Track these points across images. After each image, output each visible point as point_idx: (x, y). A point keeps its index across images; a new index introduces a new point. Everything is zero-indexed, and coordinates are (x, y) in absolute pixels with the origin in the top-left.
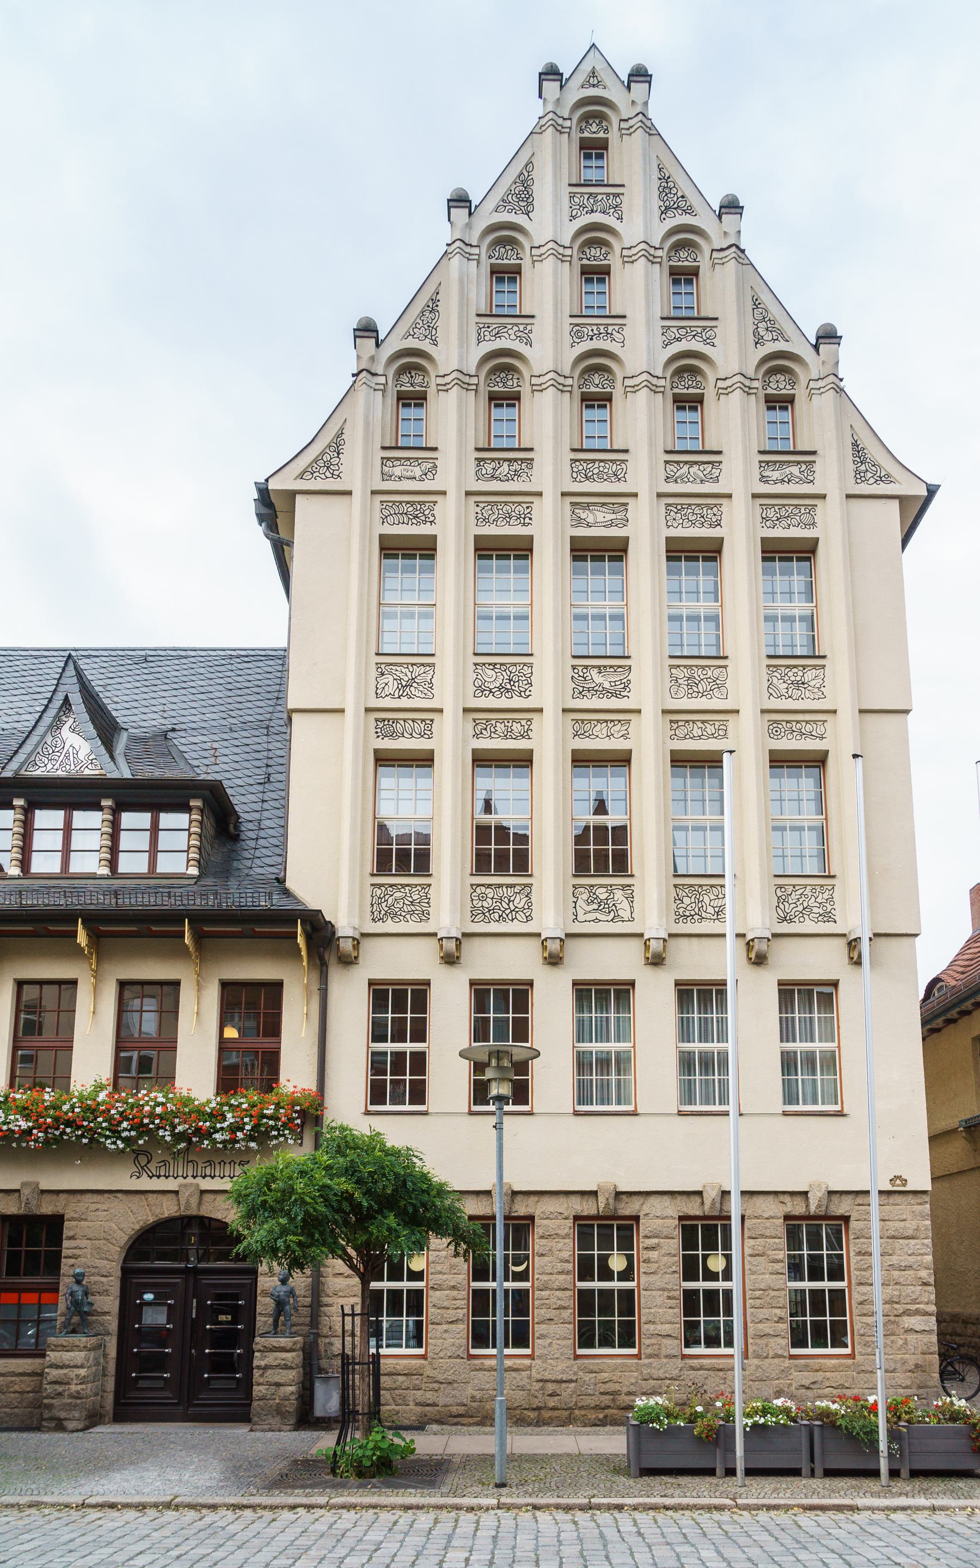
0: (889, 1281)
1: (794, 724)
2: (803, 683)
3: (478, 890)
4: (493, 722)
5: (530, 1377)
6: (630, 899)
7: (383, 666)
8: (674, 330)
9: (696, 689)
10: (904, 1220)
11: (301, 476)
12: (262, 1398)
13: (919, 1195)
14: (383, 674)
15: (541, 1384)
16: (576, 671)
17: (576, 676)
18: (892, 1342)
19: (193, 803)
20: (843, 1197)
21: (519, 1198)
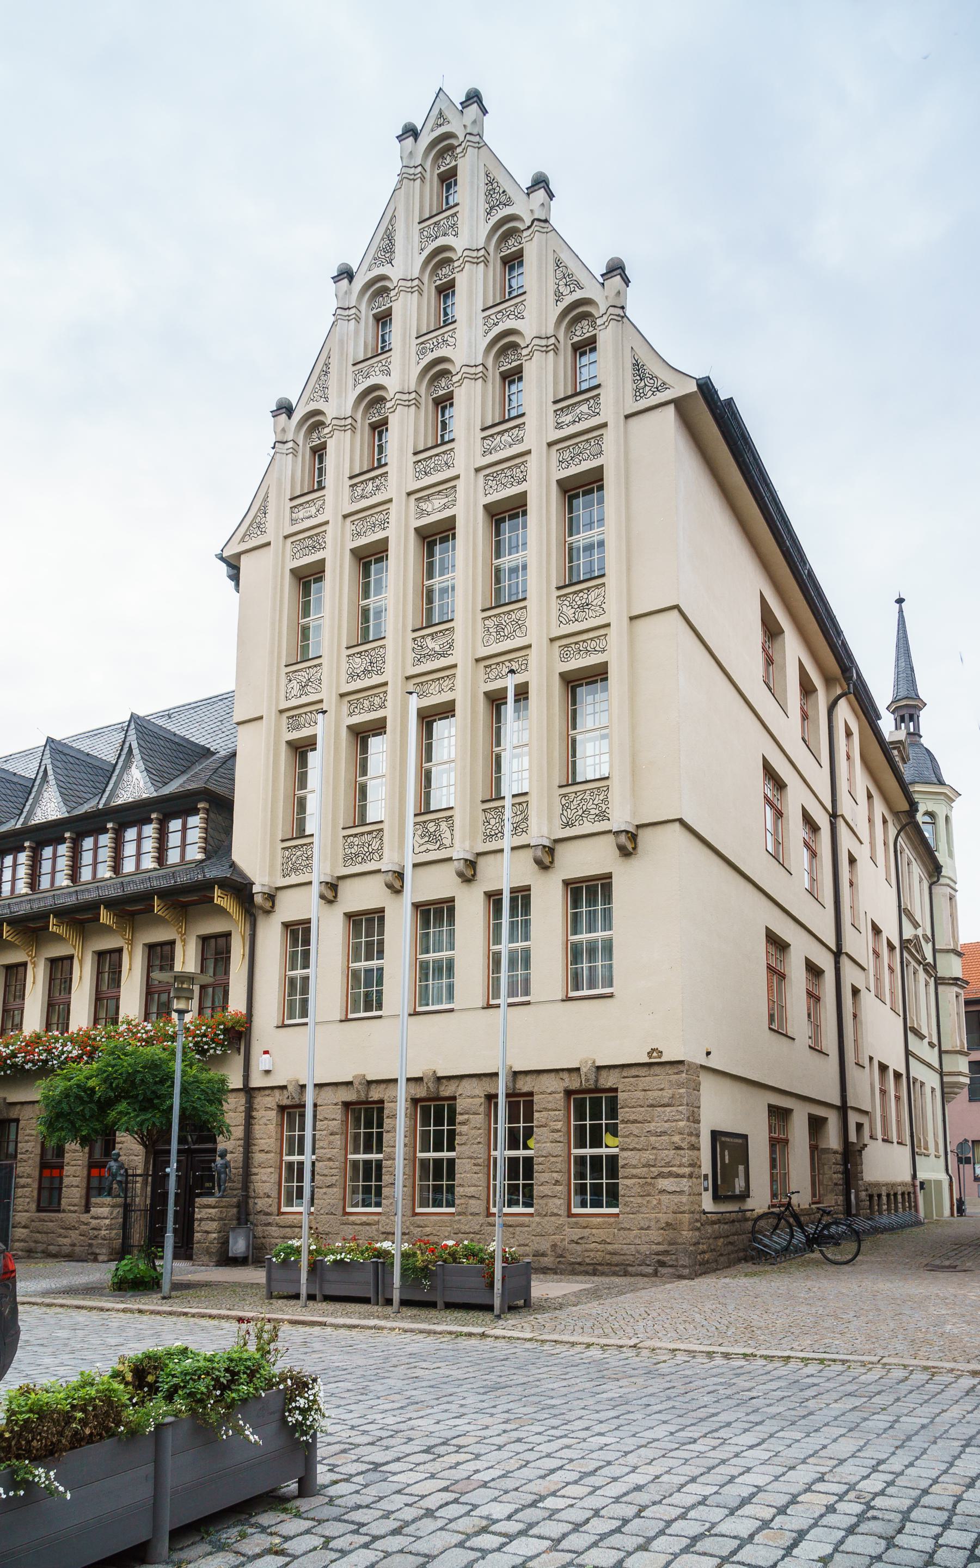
1: (589, 642)
6: (451, 828)
9: (502, 634)
10: (661, 1090)
11: (243, 540)
18: (648, 1202)
19: (200, 806)
21: (373, 1086)
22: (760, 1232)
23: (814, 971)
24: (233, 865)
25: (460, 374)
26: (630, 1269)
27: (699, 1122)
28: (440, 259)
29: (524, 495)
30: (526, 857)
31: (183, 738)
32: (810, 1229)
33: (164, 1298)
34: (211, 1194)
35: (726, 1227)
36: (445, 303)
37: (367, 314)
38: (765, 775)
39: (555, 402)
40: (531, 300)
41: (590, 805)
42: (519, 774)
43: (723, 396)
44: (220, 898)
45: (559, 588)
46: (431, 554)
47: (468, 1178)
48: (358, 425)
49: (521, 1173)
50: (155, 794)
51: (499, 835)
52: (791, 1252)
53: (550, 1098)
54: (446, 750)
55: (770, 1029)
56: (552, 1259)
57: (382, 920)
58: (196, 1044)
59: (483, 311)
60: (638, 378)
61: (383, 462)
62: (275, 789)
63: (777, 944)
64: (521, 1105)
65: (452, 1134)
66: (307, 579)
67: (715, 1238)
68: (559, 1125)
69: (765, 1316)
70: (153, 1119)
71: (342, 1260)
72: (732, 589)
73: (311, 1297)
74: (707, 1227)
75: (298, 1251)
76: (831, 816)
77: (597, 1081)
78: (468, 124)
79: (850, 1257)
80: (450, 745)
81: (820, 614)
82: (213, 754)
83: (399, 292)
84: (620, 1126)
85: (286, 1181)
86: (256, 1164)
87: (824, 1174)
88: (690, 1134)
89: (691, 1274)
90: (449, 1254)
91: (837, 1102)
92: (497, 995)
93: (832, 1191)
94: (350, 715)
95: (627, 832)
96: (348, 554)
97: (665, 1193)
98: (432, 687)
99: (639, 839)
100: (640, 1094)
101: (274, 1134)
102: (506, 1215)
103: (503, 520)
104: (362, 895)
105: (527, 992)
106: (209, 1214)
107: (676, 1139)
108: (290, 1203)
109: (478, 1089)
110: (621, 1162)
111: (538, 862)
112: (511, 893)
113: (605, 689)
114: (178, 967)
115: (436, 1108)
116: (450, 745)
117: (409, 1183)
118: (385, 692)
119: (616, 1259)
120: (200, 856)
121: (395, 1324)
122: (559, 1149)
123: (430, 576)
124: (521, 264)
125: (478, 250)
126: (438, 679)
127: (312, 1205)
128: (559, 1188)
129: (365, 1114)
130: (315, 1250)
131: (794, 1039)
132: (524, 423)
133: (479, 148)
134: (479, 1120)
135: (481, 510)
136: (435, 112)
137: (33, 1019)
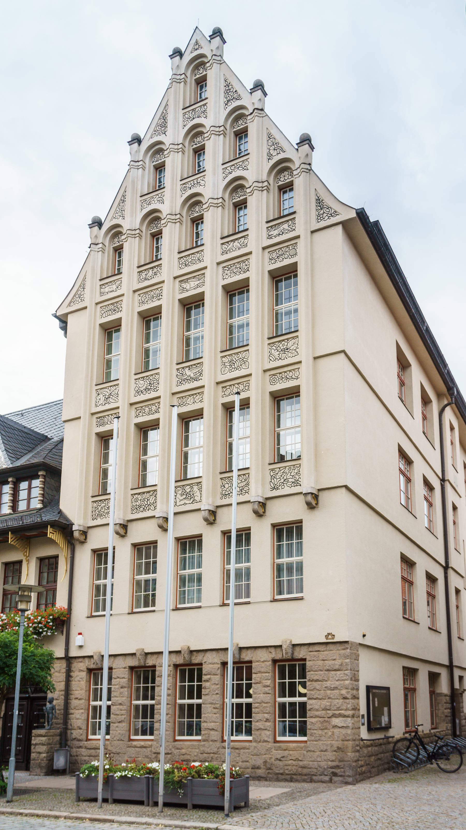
0: (325, 696)
2: (287, 349)
3: (135, 497)
4: (144, 408)
5: (151, 751)
6: (200, 490)
7: (99, 390)
8: (229, 168)
9: (233, 367)
10: (334, 660)
11: (69, 305)
12: (34, 760)
13: (343, 644)
14: (99, 395)
15: (155, 755)
16: (179, 371)
17: (179, 374)
18: (326, 733)
19: (40, 473)
20: (302, 647)
21: (149, 656)
22: (397, 751)
23: (431, 579)
24: (60, 512)
25: (208, 204)
26: (314, 778)
27: (357, 680)
28: (196, 132)
29: (248, 279)
30: (248, 509)
31: (29, 429)
32: (430, 748)
33: (8, 802)
34: (43, 727)
35: (376, 748)
36: (199, 159)
37: (149, 165)
38: (400, 455)
39: (267, 222)
40: (253, 159)
41: (289, 476)
42: (244, 455)
43: (372, 219)
44: (51, 534)
45: (269, 339)
46: (189, 316)
47: (209, 718)
48: (143, 234)
49: (244, 712)
50: (11, 466)
51: (231, 494)
52: (418, 763)
53: (263, 665)
54: (197, 440)
55: (404, 618)
56: (264, 771)
57: (156, 548)
58: (35, 628)
59: (223, 164)
60: (319, 208)
61: (159, 258)
62: (88, 463)
63: (407, 562)
64: (243, 669)
65: (200, 688)
66: (110, 330)
67: (369, 756)
68: (269, 682)
69: (401, 814)
70: (4, 681)
71: (126, 776)
72: (379, 340)
73: (105, 800)
74: (364, 749)
75: (96, 769)
76: (441, 480)
77: (293, 654)
78: (214, 49)
79: (456, 767)
80: (200, 437)
81: (434, 355)
82: (50, 439)
83: (170, 152)
84: (308, 684)
85: (92, 719)
86: (72, 707)
87: (439, 710)
88: (353, 689)
89: (353, 781)
90: (196, 772)
91: (447, 663)
92: (228, 598)
93: (444, 720)
94: (137, 416)
95: (312, 494)
96: (136, 315)
97: (337, 728)
98: (189, 400)
99: (320, 498)
100: (320, 663)
101: (84, 687)
102: (233, 741)
103: (234, 295)
104: (143, 532)
105: (248, 596)
106: (40, 740)
107: (344, 692)
108: (94, 734)
109: (216, 659)
110: (308, 707)
111: (256, 512)
112: (237, 532)
113: (298, 402)
114: (23, 582)
115: (189, 671)
116: (200, 437)
117: (172, 720)
118: (159, 403)
119: (305, 771)
120: (39, 506)
121: (159, 821)
122: (268, 698)
123: (188, 329)
124: (246, 136)
125: (220, 127)
126: (193, 395)
127: (108, 733)
128: (268, 724)
129: (144, 674)
130: (109, 769)
131: (419, 624)
132: (248, 235)
133: (221, 64)
134: (217, 679)
135: (220, 289)
136: (193, 41)
137: (6, 510)
